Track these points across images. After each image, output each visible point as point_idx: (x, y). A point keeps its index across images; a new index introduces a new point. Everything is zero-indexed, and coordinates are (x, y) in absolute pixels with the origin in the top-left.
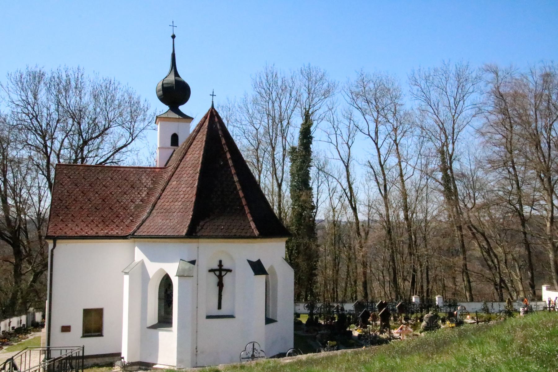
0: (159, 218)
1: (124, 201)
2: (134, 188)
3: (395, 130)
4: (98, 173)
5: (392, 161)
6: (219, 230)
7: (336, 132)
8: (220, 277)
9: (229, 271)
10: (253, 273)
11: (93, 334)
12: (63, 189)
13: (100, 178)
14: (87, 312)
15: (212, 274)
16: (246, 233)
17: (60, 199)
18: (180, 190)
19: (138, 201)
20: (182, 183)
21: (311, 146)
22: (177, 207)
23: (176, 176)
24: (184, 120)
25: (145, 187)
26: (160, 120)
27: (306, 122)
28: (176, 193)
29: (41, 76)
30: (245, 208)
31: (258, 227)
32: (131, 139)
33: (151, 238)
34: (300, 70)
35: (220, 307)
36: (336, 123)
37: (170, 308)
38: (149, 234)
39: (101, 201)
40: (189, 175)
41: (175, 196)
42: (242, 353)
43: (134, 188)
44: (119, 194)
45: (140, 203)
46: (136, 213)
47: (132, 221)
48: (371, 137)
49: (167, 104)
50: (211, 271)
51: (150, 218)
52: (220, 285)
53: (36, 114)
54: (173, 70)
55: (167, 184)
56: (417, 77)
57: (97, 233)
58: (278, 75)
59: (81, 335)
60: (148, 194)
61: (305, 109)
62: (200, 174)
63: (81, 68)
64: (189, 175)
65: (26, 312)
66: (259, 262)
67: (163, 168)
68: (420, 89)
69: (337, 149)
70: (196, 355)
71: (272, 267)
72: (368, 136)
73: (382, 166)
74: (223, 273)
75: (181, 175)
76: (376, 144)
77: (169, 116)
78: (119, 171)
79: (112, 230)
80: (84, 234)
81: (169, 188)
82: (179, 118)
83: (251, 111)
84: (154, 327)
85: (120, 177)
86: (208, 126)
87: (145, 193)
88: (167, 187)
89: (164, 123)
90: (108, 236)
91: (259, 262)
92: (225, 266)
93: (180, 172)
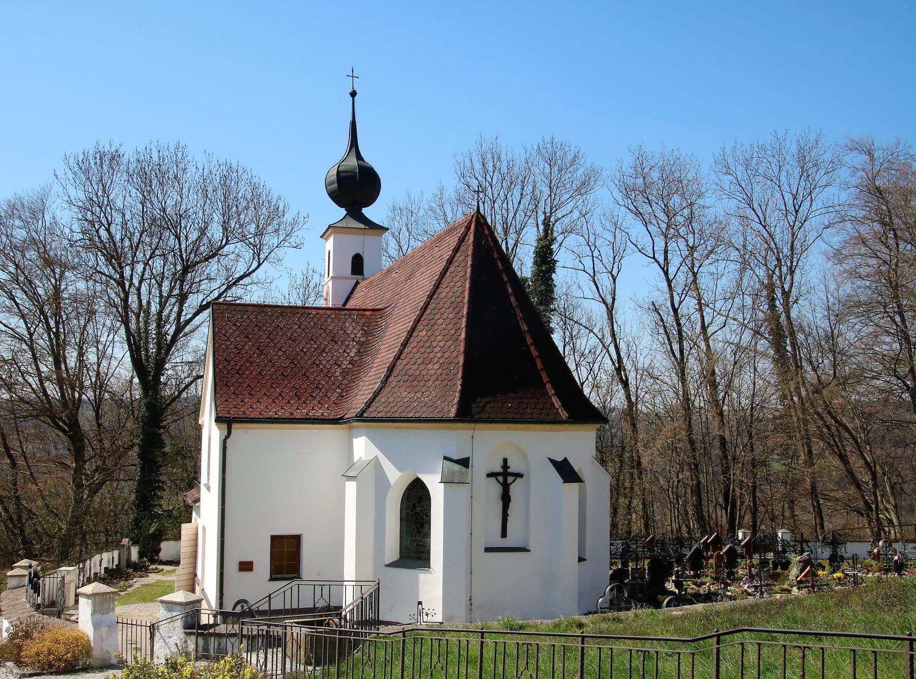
2: (336, 342)
3: (692, 249)
5: (689, 306)
8: (506, 487)
9: (520, 475)
11: (286, 576)
13: (282, 325)
14: (276, 540)
15: (493, 479)
16: (548, 415)
18: (435, 345)
20: (437, 333)
21: (554, 276)
23: (425, 322)
24: (372, 231)
27: (546, 235)
29: (115, 158)
30: (542, 375)
31: (565, 406)
32: (255, 264)
33: (394, 421)
34: (536, 148)
35: (504, 534)
37: (425, 530)
40: (448, 321)
42: (600, 600)
43: (336, 342)
44: (314, 351)
46: (345, 382)
47: (340, 396)
48: (658, 262)
50: (490, 475)
51: (387, 390)
52: (506, 499)
53: (107, 220)
54: (354, 149)
55: (411, 336)
56: (730, 160)
57: (292, 414)
58: (503, 157)
59: (269, 578)
61: (545, 213)
64: (448, 321)
65: (118, 545)
66: (566, 460)
67: (339, 309)
68: (735, 181)
69: (594, 281)
71: (579, 469)
72: (653, 260)
73: (675, 310)
74: (510, 479)
76: (666, 274)
78: (309, 314)
81: (413, 343)
84: (393, 565)
85: (312, 323)
86: (474, 242)
87: (354, 350)
89: (335, 235)
91: (566, 460)
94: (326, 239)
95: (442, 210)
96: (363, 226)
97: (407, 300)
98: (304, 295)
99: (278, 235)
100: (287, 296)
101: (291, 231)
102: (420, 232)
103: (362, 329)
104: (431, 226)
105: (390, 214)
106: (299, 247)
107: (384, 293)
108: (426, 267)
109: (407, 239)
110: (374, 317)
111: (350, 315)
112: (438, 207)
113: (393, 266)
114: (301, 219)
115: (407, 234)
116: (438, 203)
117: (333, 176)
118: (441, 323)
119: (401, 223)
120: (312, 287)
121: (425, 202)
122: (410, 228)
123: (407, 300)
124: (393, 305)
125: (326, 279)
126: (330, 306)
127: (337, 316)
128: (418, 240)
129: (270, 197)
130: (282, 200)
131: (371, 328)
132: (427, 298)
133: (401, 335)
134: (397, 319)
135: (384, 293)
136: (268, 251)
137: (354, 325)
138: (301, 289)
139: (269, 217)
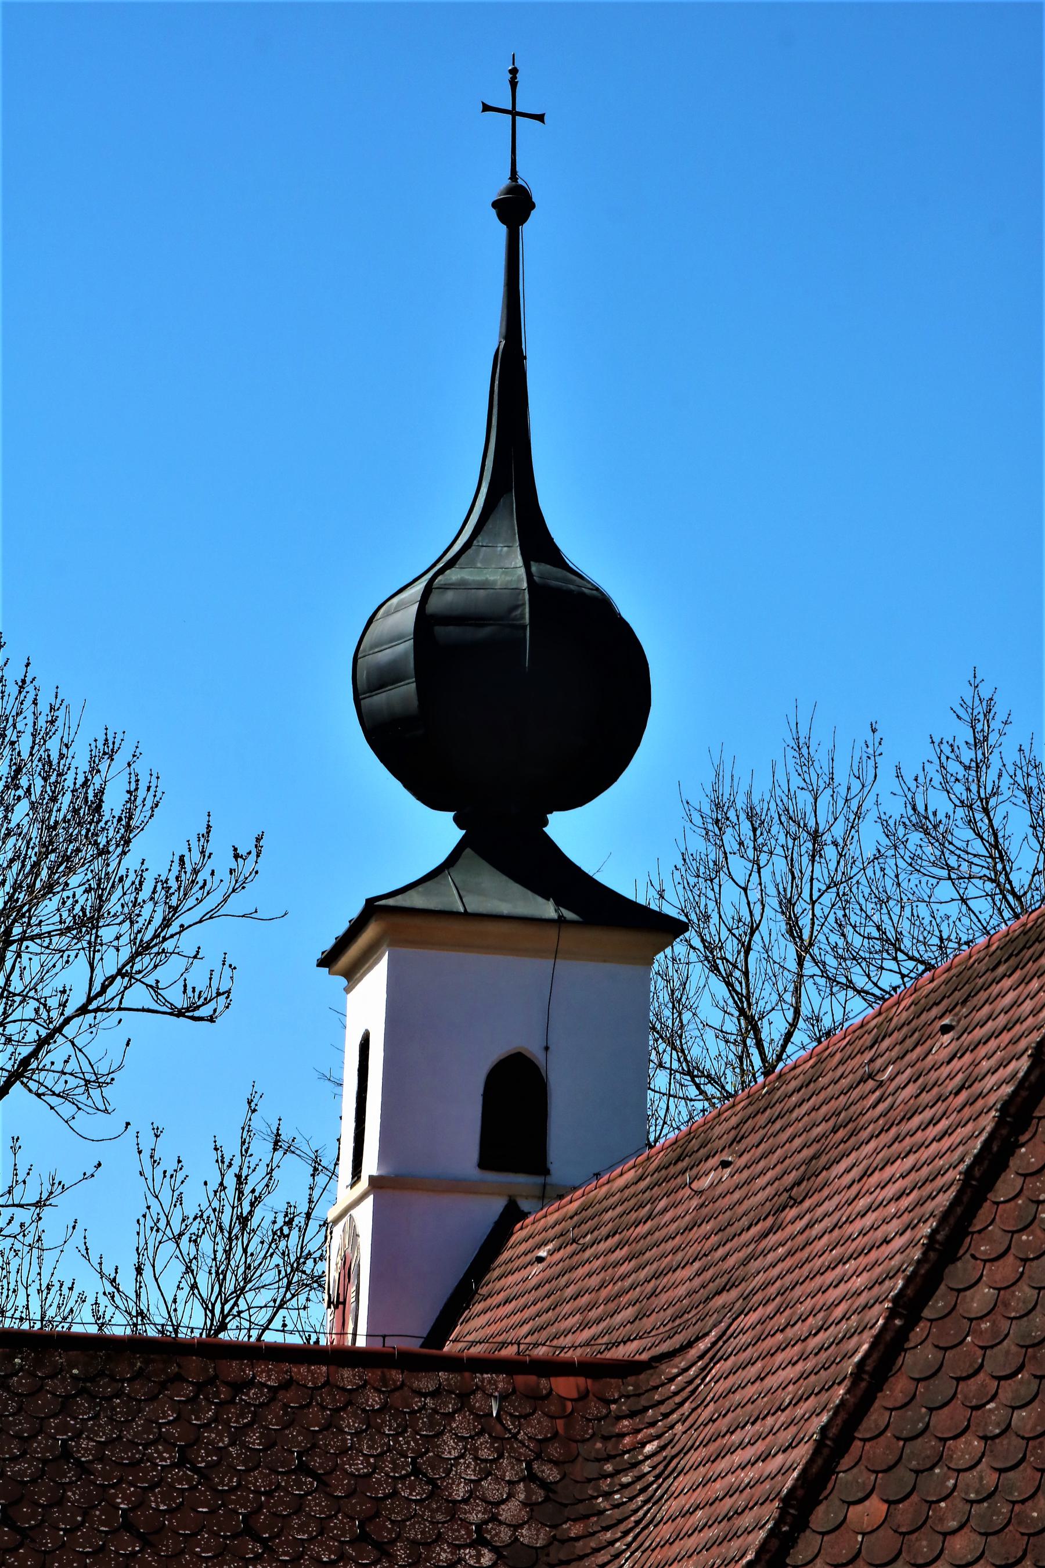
4: (66, 1405)
23: (880, 1451)
25: (480, 1542)
26: (392, 939)
55: (801, 1524)
67: (407, 1361)
73: (263, 1287)
75: (927, 1445)
77: (475, 904)
78: (240, 1386)
82: (561, 921)
83: (119, 850)
85: (254, 1441)
89: (408, 952)
94: (352, 975)
95: (983, 825)
96: (548, 910)
97: (781, 1320)
98: (220, 1277)
99: (93, 947)
100: (127, 1283)
101: (166, 923)
102: (857, 941)
103: (531, 1477)
104: (923, 910)
105: (698, 845)
106: (205, 1011)
107: (656, 1276)
108: (886, 1138)
109: (787, 980)
110: (594, 1408)
111: (464, 1398)
112: (961, 812)
113: (709, 1125)
114: (221, 861)
115: (786, 952)
116: (959, 788)
117: (396, 639)
118: (966, 1460)
119: (754, 895)
120: (265, 1231)
121: (887, 782)
122: (805, 921)
123: (781, 1320)
124: (702, 1346)
125: (344, 1192)
126: (361, 1342)
127: (396, 1398)
128: (850, 985)
129: (54, 746)
130: (122, 758)
131: (583, 1470)
132: (892, 1314)
133: (747, 1520)
134: (723, 1424)
135: (656, 1276)
136: (33, 1033)
137: (485, 1454)
138: (206, 1244)
139: (47, 847)
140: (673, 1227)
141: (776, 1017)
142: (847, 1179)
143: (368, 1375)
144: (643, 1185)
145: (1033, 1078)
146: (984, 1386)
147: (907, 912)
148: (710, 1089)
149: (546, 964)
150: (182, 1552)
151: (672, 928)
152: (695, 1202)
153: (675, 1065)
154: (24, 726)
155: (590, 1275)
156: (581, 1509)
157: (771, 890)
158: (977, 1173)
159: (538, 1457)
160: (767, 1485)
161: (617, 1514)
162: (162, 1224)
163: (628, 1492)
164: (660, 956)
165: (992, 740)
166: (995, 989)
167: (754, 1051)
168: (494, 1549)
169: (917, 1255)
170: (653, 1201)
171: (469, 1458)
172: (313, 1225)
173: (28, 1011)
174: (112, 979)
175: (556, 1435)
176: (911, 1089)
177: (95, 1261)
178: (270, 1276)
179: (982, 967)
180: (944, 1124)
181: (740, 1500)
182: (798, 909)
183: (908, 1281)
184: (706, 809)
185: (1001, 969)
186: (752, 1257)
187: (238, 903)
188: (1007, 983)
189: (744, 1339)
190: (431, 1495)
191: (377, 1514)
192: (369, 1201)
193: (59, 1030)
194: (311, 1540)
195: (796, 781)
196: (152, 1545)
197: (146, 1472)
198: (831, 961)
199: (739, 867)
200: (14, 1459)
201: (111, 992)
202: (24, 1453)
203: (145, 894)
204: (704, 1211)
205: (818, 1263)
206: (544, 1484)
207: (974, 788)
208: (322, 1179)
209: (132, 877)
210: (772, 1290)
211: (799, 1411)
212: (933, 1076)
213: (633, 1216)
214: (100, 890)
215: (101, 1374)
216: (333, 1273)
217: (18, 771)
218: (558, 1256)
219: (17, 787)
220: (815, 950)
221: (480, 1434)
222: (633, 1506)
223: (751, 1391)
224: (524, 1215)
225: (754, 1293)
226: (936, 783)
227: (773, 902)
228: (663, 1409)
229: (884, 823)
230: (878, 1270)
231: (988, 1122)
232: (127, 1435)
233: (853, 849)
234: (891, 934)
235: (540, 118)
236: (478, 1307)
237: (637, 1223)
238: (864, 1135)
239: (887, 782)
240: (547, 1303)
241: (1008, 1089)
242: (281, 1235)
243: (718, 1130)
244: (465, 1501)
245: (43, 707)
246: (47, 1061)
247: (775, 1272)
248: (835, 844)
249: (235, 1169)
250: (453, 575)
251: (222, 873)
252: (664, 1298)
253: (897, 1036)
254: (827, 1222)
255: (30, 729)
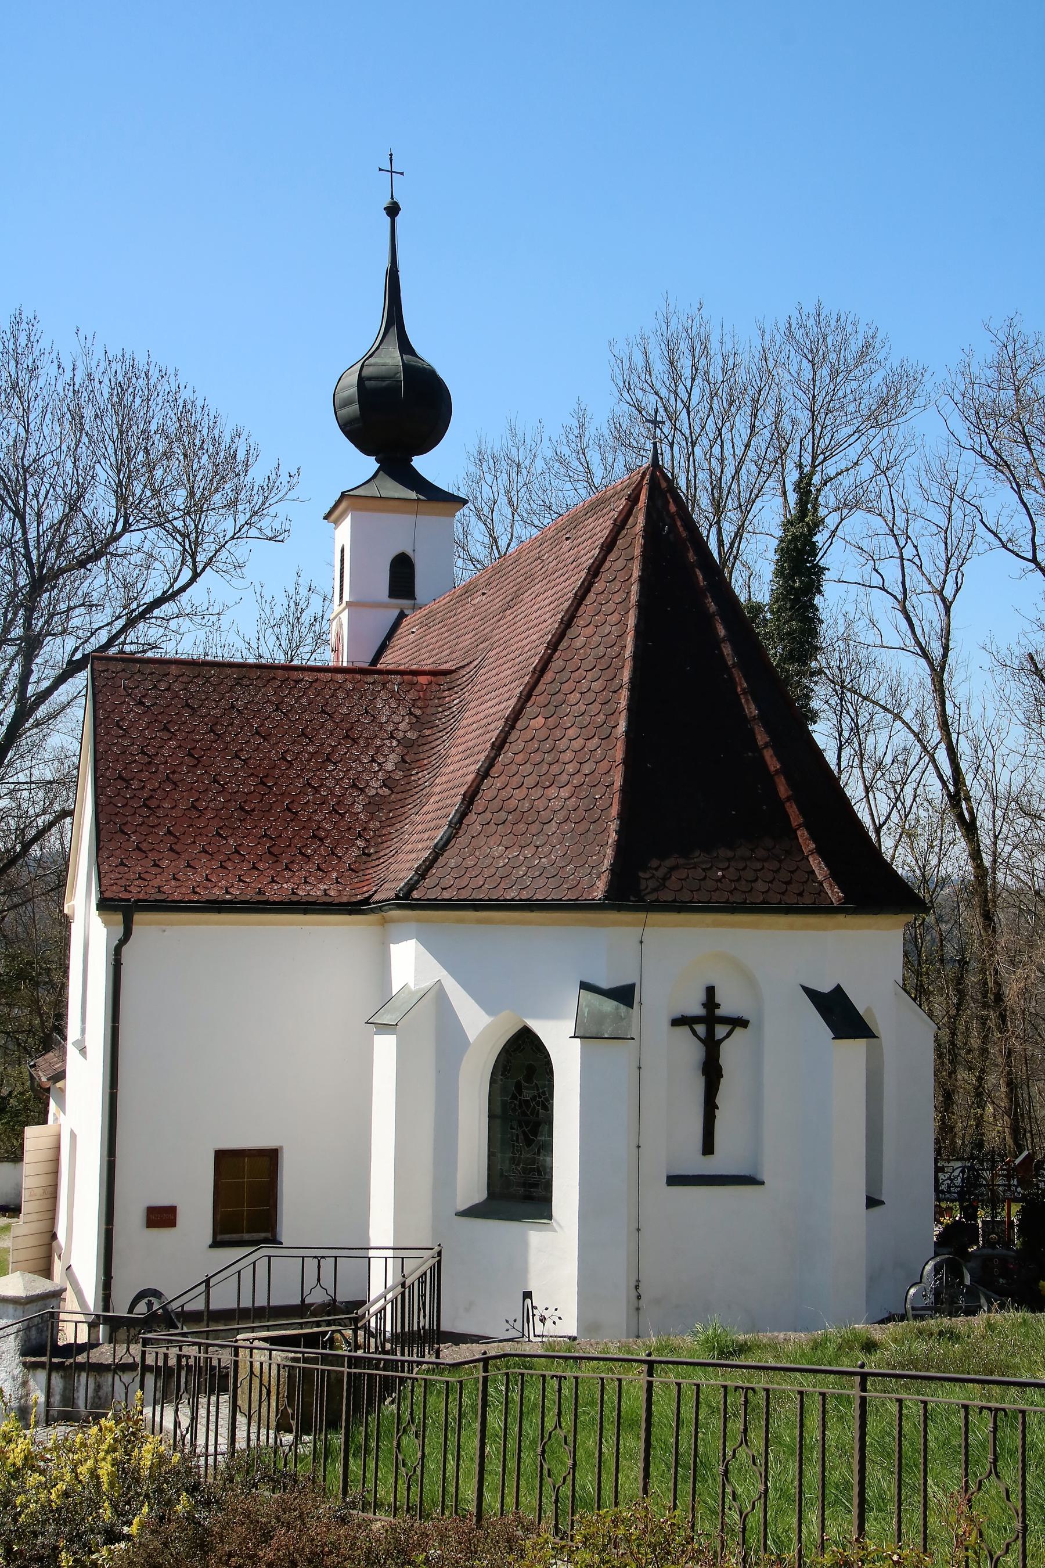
0: (492, 841)
1: (330, 784)
2: (355, 741)
4: (231, 688)
6: (710, 884)
7: (901, 549)
9: (740, 1023)
10: (829, 1033)
11: (246, 1236)
12: (127, 743)
17: (120, 777)
18: (562, 747)
19: (373, 784)
20: (567, 721)
21: (818, 600)
22: (556, 804)
23: (542, 699)
24: (441, 505)
26: (353, 508)
27: (803, 512)
28: (549, 758)
31: (836, 876)
32: (186, 574)
35: (708, 1148)
36: (900, 521)
38: (464, 894)
39: (252, 781)
40: (590, 696)
41: (545, 767)
43: (355, 741)
45: (380, 791)
47: (364, 854)
49: (367, 452)
51: (461, 841)
54: (394, 330)
55: (513, 727)
57: (260, 892)
58: (714, 346)
59: (209, 1240)
60: (404, 761)
62: (631, 690)
63: (28, 314)
64: (590, 696)
67: (362, 671)
70: (638, 1309)
72: (1032, 566)
74: (721, 1031)
75: (560, 697)
78: (297, 682)
79: (306, 882)
80: (217, 893)
85: (304, 702)
87: (394, 758)
88: (511, 739)
90: (298, 903)
92: (727, 1007)
93: (556, 686)
94: (337, 522)
95: (583, 460)
96: (413, 495)
97: (505, 652)
99: (235, 513)
101: (263, 503)
102: (535, 507)
103: (411, 714)
104: (560, 494)
105: (473, 469)
106: (280, 538)
107: (457, 637)
108: (545, 582)
109: (508, 523)
110: (435, 688)
111: (384, 684)
112: (574, 455)
114: (284, 478)
115: (508, 511)
116: (573, 445)
118: (575, 701)
119: (495, 489)
121: (546, 443)
122: (515, 499)
123: (505, 652)
124: (475, 663)
125: (336, 607)
126: (345, 664)
129: (216, 432)
130: (243, 437)
132: (547, 648)
133: (493, 726)
134: (483, 692)
135: (457, 637)
136: (213, 547)
137: (393, 705)
139: (216, 473)
140: (464, 619)
141: (504, 537)
142: (530, 598)
143: (347, 677)
144: (452, 603)
145: (600, 557)
146: (581, 674)
147: (554, 495)
148: (479, 566)
149: (412, 517)
150: (279, 742)
151: (464, 502)
152: (472, 609)
153: (465, 557)
154: (205, 424)
155: (432, 638)
156: (430, 725)
157: (502, 487)
158: (579, 594)
159: (413, 706)
160: (500, 714)
161: (444, 726)
162: (267, 622)
163: (447, 718)
164: (458, 513)
165: (586, 426)
166: (586, 522)
167: (496, 551)
168: (398, 740)
169: (556, 626)
170: (456, 609)
171: (387, 707)
172: (325, 621)
173: (211, 538)
174: (243, 525)
175: (420, 698)
176: (555, 562)
177: (242, 636)
178: (309, 641)
179: (581, 514)
180: (567, 575)
181: (489, 720)
182: (512, 494)
183: (553, 635)
184: (475, 455)
185: (589, 514)
186: (494, 629)
187: (291, 495)
188: (590, 520)
189: (491, 660)
190: (372, 721)
191: (352, 728)
192: (346, 611)
193: (224, 546)
194: (327, 737)
195: (511, 443)
196: (267, 740)
197: (264, 713)
198: (525, 515)
199: (489, 478)
200: (213, 708)
201: (243, 531)
202: (217, 706)
203: (255, 492)
204: (476, 612)
205: (519, 630)
206: (416, 716)
207: (579, 445)
208: (327, 603)
209: (249, 485)
210: (502, 641)
211: (512, 686)
212: (563, 557)
213: (449, 615)
214: (237, 491)
215: (245, 677)
216: (333, 640)
217: (203, 443)
218: (420, 631)
219: (203, 449)
220: (518, 510)
221: (391, 698)
222: (450, 723)
223: (494, 679)
224: (407, 616)
225: (495, 642)
226: (565, 443)
227: (502, 491)
228: (461, 687)
229: (545, 460)
230: (542, 632)
231: (583, 574)
232: (256, 700)
233: (533, 470)
234: (548, 504)
235: (402, 174)
236: (389, 652)
237: (450, 618)
238: (537, 581)
239: (546, 443)
240: (416, 649)
241: (591, 561)
242: (312, 625)
243: (481, 581)
244: (386, 723)
245: (212, 417)
246: (219, 558)
247: (502, 635)
248: (526, 468)
249: (293, 599)
250: (372, 360)
251: (285, 483)
252: (461, 646)
253: (549, 542)
254: (523, 615)
255: (207, 426)
